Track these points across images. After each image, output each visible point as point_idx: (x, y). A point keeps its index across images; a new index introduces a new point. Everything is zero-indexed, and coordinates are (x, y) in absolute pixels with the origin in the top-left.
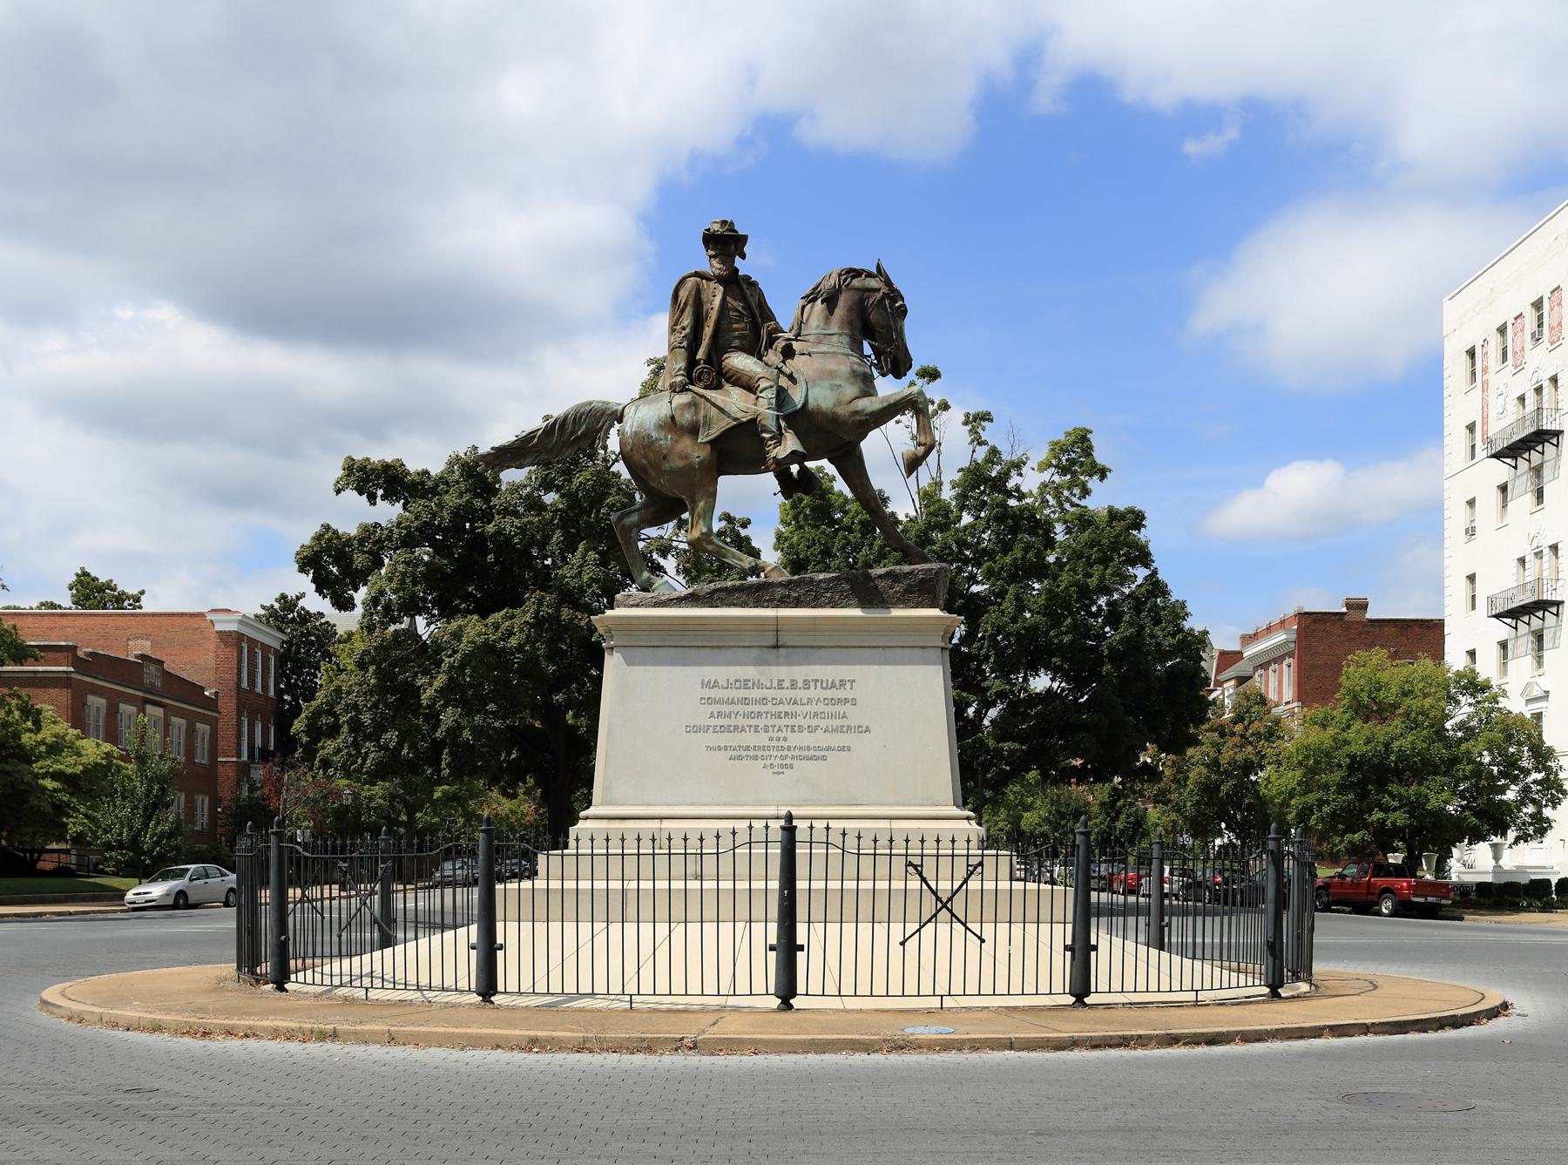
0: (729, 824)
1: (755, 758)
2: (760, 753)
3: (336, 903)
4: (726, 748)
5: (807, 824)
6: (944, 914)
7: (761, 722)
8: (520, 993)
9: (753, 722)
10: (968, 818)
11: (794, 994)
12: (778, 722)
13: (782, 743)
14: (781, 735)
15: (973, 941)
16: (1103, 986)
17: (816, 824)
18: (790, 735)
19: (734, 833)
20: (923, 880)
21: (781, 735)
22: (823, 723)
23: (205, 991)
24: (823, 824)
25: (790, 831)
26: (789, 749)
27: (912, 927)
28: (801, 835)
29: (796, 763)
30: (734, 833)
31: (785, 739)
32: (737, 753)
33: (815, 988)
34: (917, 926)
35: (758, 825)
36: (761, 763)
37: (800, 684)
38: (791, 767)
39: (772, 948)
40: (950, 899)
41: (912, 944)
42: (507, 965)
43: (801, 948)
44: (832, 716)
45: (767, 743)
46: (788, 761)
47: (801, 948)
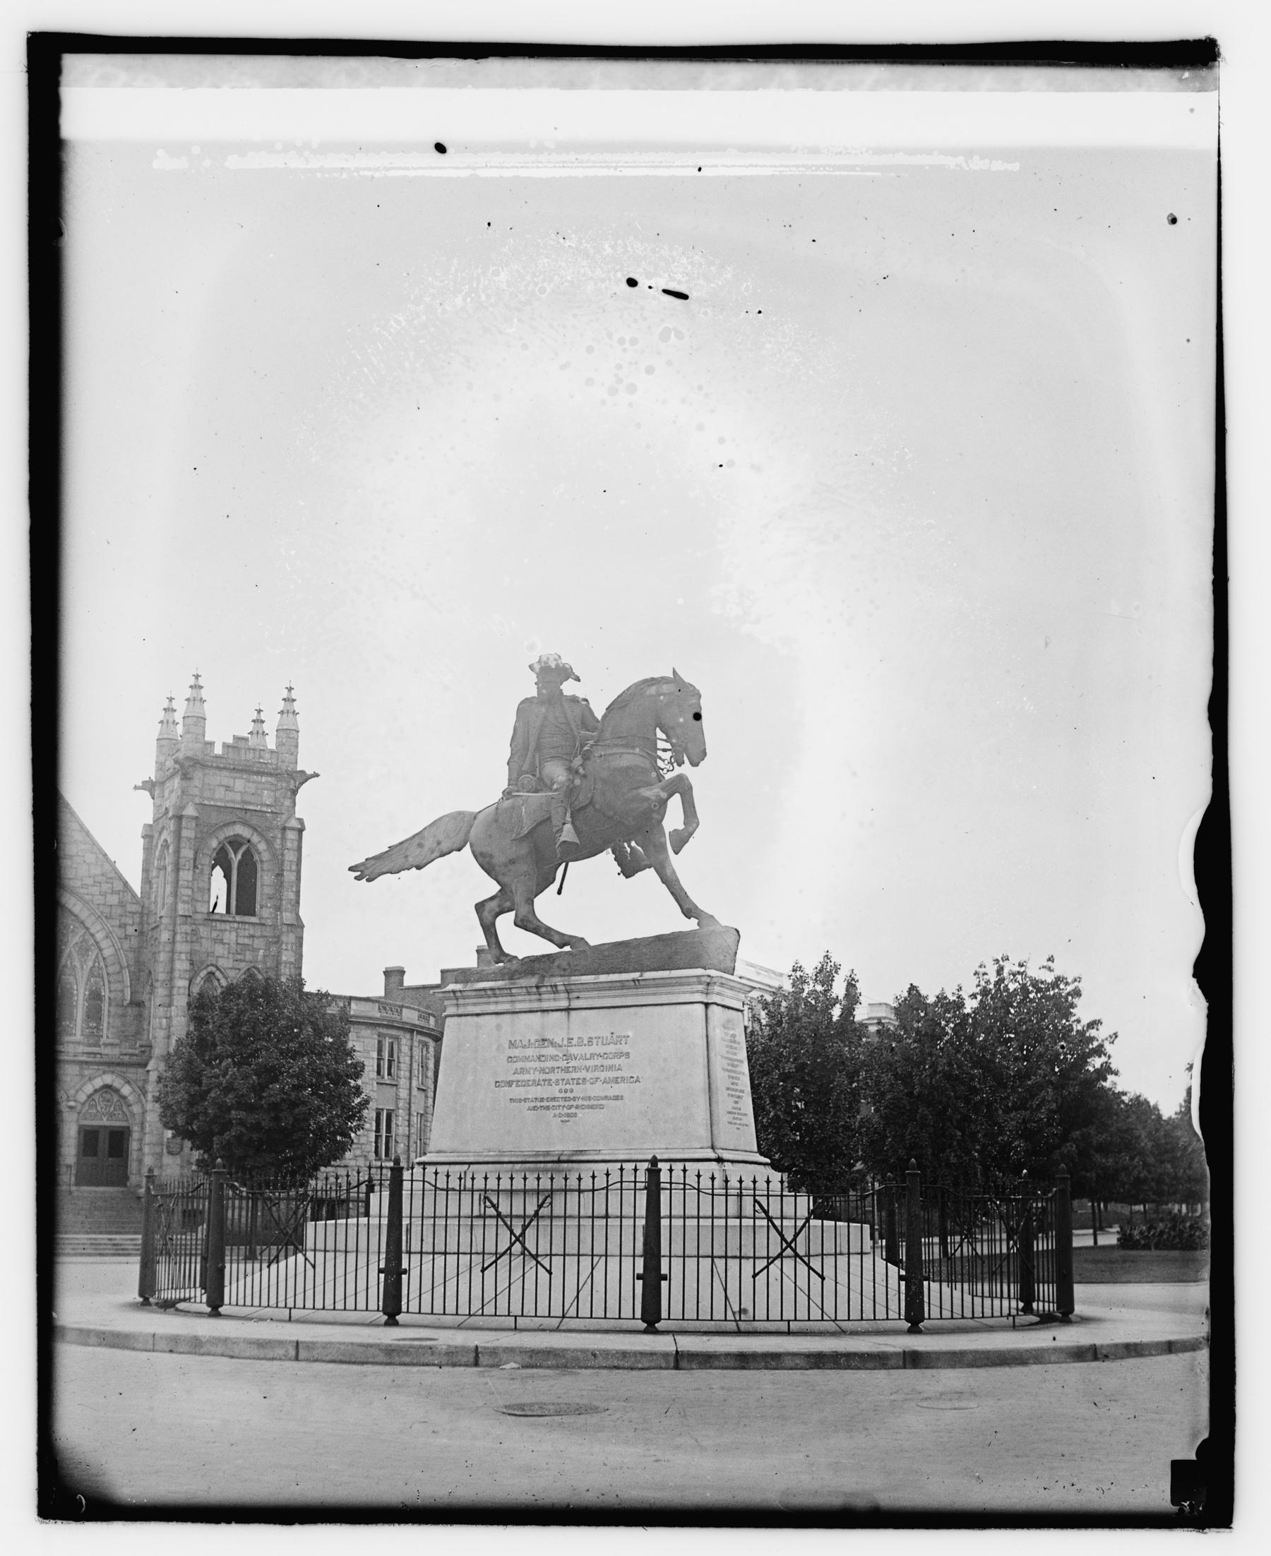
0: (603, 1166)
1: (548, 1108)
2: (551, 1104)
3: (691, 1223)
4: (525, 1100)
5: (667, 1166)
6: (789, 1252)
7: (553, 1077)
8: (963, 1317)
9: (547, 1077)
10: (765, 1164)
11: (399, 1312)
12: (567, 1076)
13: (568, 1095)
14: (568, 1087)
15: (543, 1274)
16: (414, 1307)
17: (625, 1165)
18: (574, 1087)
19: (608, 1175)
20: (770, 1219)
21: (568, 1087)
22: (603, 1075)
23: (1122, 1321)
24: (632, 1165)
25: (654, 1173)
26: (574, 1099)
27: (761, 1264)
28: (664, 1177)
29: (580, 1113)
30: (608, 1175)
31: (572, 1091)
32: (533, 1104)
33: (676, 1312)
34: (764, 1262)
35: (629, 1167)
36: (552, 1112)
37: (586, 1042)
38: (575, 1115)
39: (639, 1277)
40: (794, 1239)
41: (762, 1278)
42: (410, 1286)
43: (405, 1272)
44: (611, 1068)
45: (558, 1095)
46: (573, 1110)
47: (405, 1272)
